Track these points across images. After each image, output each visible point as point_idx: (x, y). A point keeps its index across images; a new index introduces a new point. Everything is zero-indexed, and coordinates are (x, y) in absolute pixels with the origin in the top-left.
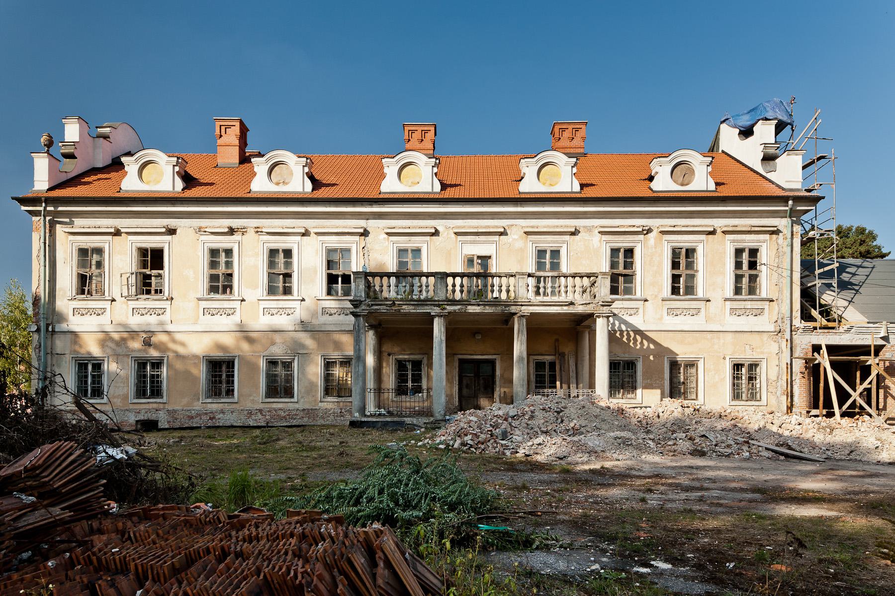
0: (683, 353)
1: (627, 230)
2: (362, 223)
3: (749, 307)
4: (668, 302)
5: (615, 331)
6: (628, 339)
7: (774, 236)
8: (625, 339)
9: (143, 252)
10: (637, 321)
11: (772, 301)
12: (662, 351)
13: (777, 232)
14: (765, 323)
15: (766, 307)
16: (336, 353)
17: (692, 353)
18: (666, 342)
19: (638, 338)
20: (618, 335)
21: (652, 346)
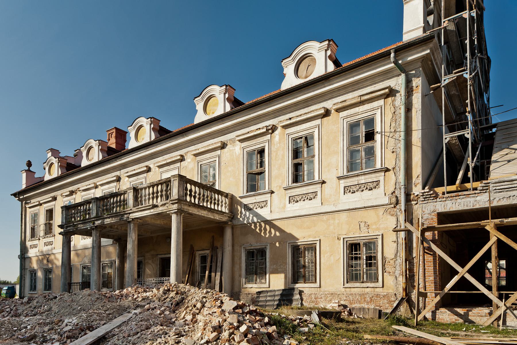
0: (303, 235)
1: (255, 133)
2: (52, 194)
3: (363, 182)
4: (289, 191)
5: (251, 224)
6: (260, 230)
7: (390, 100)
8: (258, 230)
9: (47, 211)
10: (265, 213)
11: (387, 170)
12: (286, 237)
13: (392, 93)
14: (379, 197)
15: (382, 179)
16: (107, 260)
17: (309, 236)
18: (288, 228)
19: (268, 227)
20: (253, 227)
21: (278, 234)
